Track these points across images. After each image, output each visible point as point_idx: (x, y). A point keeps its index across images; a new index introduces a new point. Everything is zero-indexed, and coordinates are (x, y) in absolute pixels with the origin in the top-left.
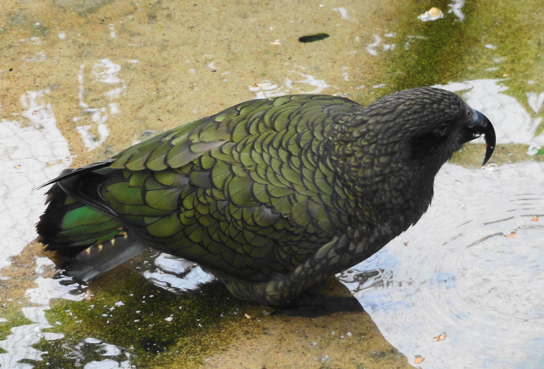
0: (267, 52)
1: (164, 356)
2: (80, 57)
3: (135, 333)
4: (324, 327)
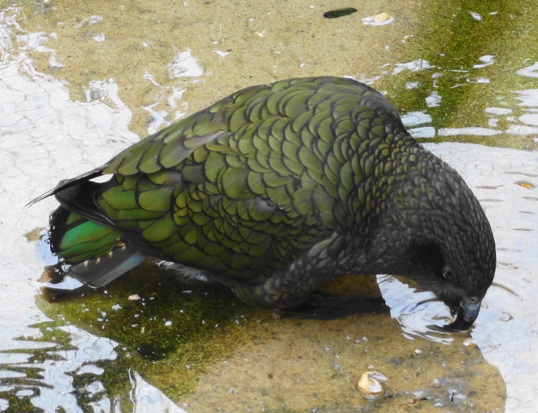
0: (288, 29)
1: (164, 364)
2: (84, 36)
3: (133, 338)
4: (338, 331)
